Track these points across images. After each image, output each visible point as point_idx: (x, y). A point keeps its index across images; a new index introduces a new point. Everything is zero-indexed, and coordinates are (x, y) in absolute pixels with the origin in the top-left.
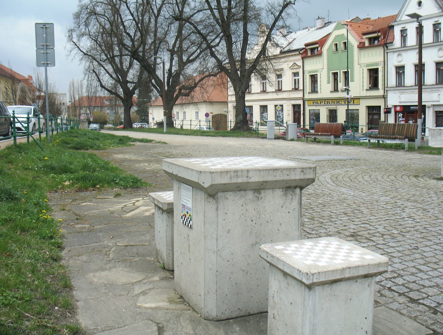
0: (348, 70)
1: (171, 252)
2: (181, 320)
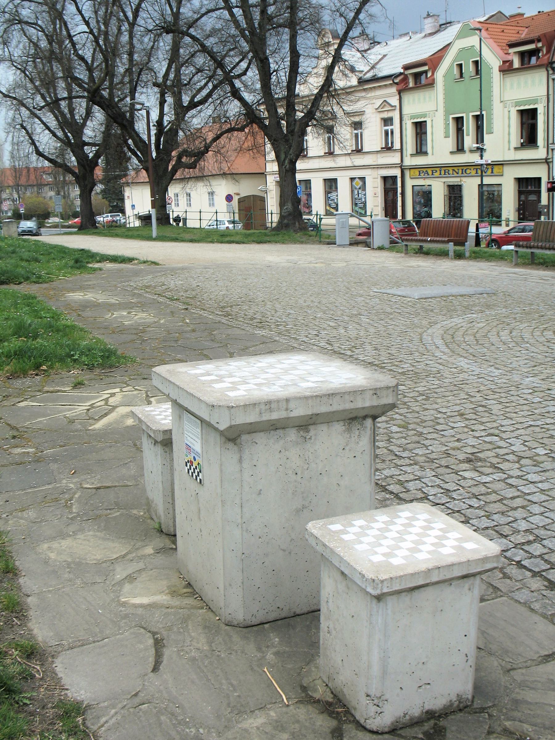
0: (481, 112)
1: (170, 506)
2: (190, 627)
